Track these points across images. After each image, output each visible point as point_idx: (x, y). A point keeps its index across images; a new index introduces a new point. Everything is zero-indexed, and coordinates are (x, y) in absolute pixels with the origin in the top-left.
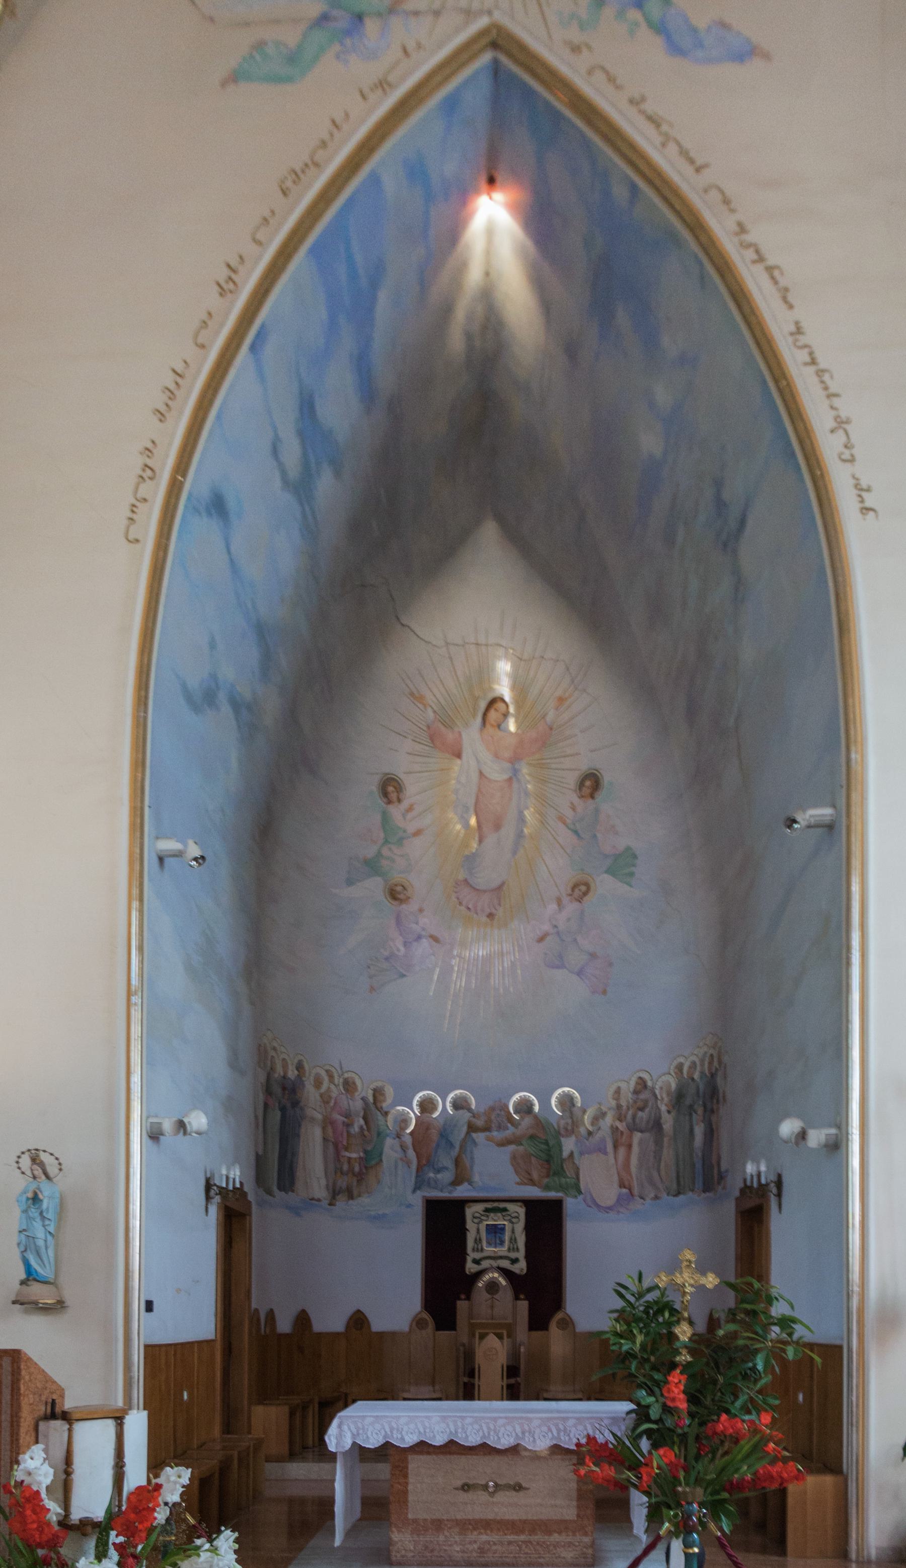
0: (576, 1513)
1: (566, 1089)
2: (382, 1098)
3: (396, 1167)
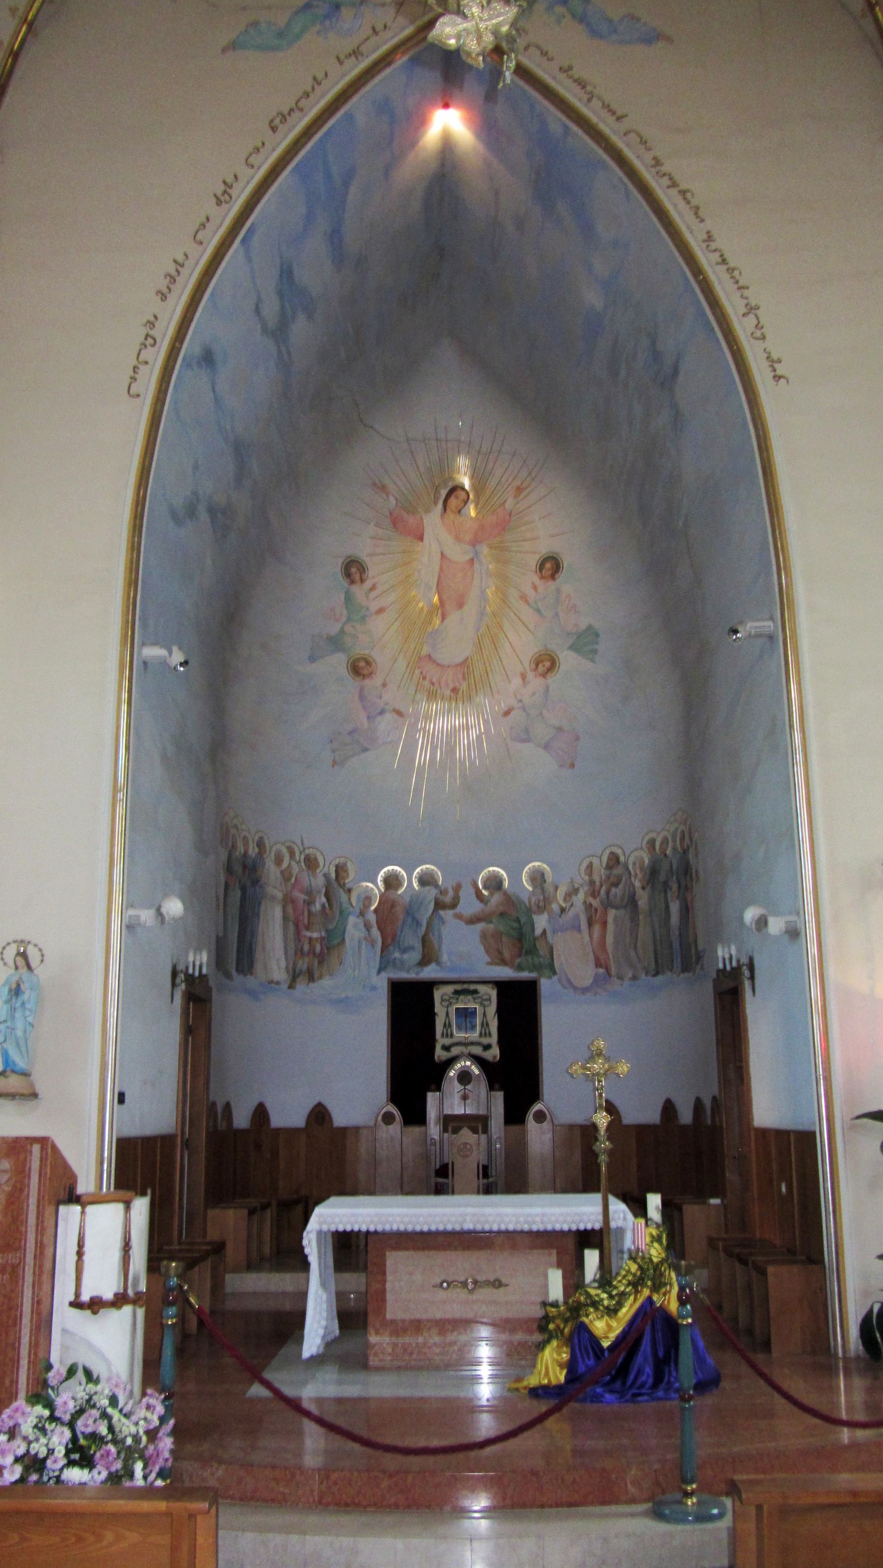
1: (537, 864)
3: (359, 947)
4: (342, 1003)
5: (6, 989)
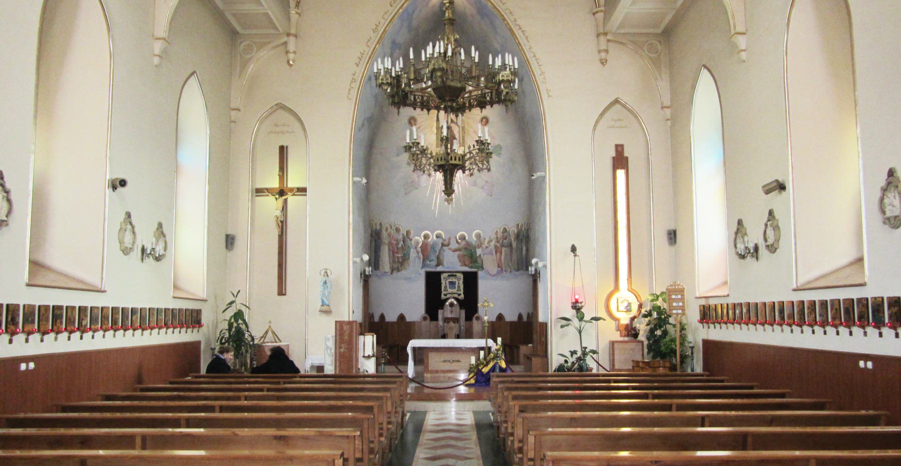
3: (415, 259)
4: (408, 279)
5: (322, 282)
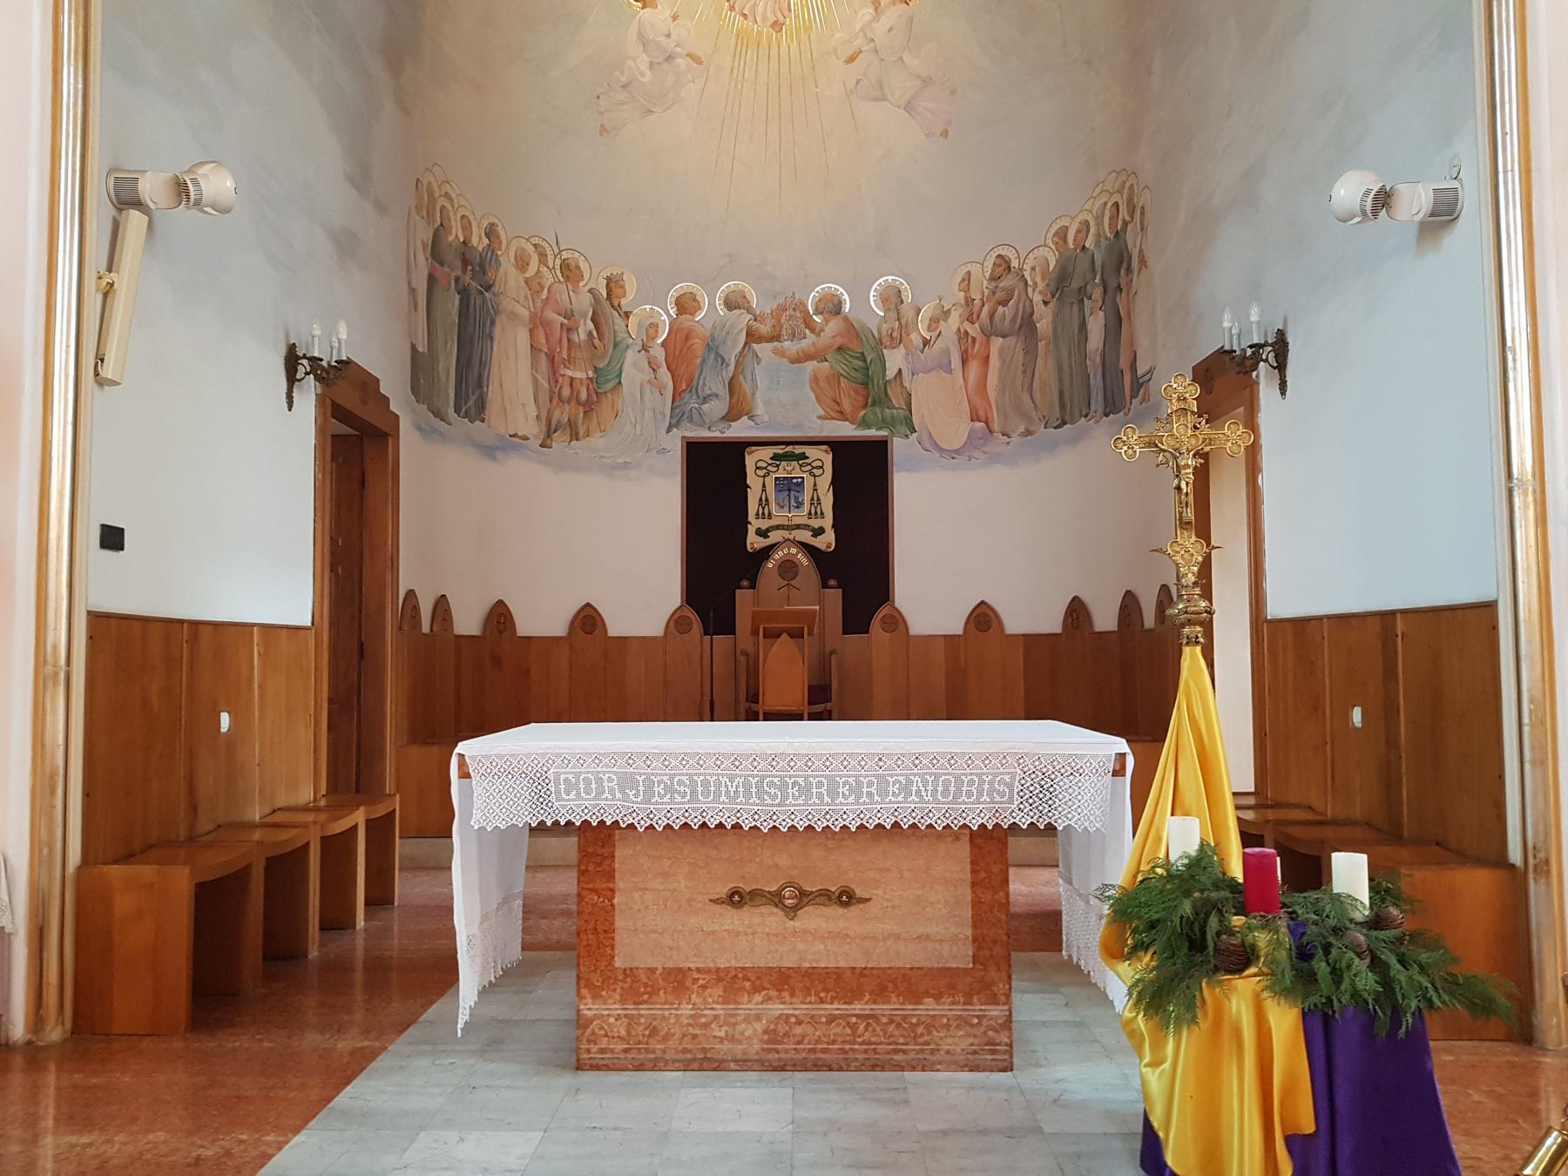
0: (971, 953)
2: (620, 291)
